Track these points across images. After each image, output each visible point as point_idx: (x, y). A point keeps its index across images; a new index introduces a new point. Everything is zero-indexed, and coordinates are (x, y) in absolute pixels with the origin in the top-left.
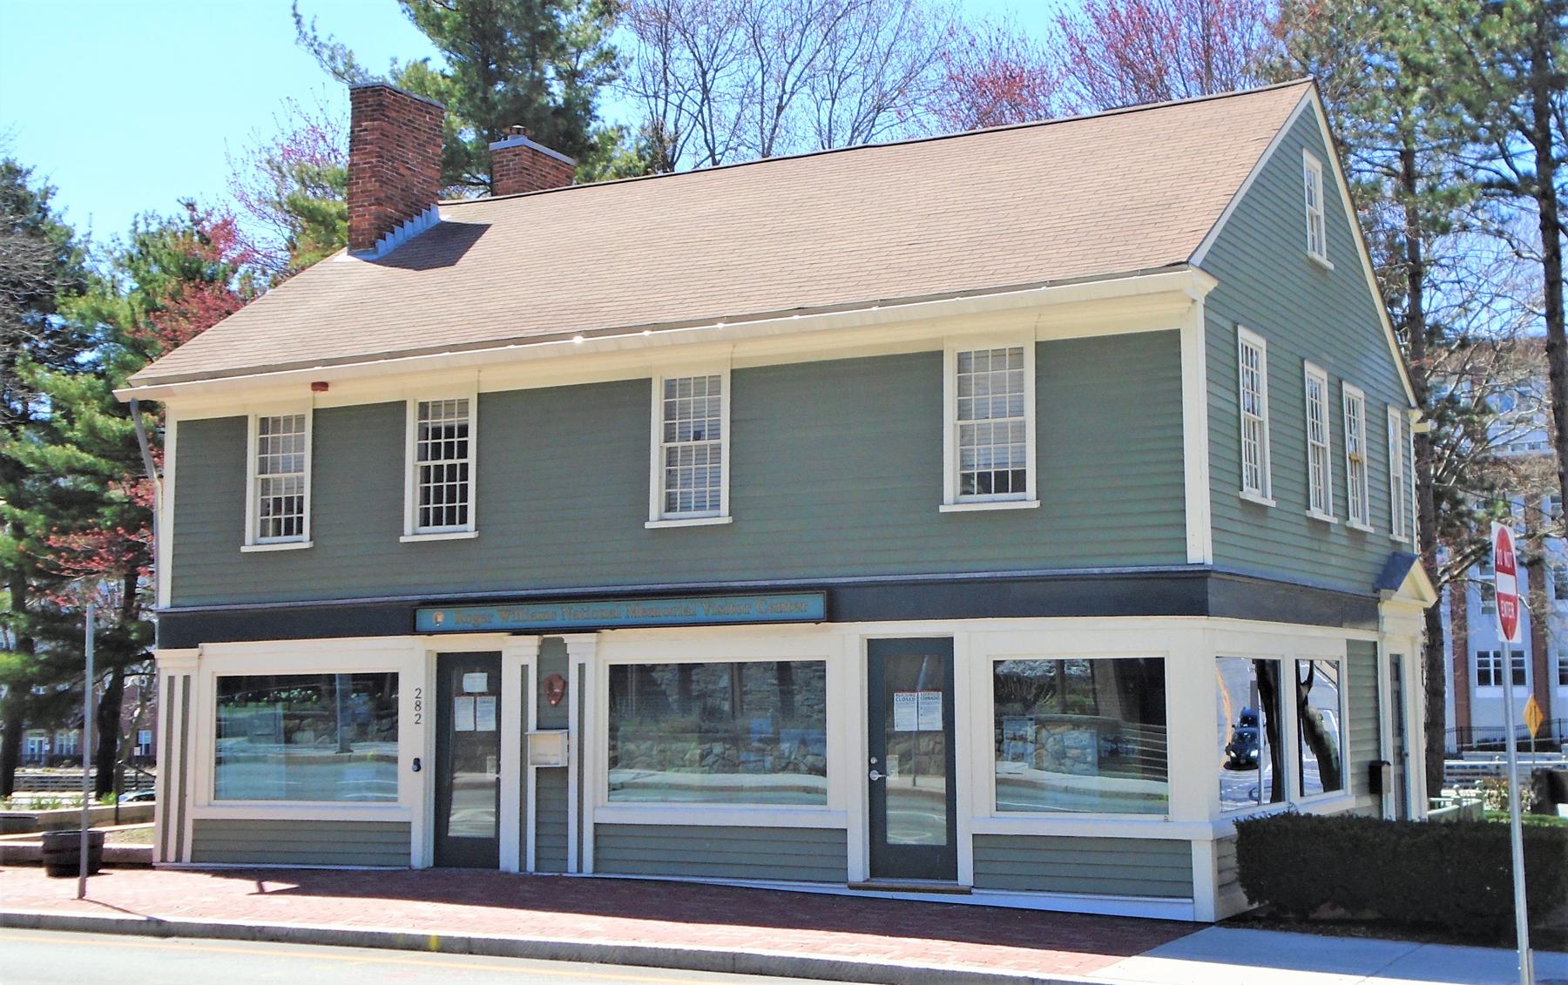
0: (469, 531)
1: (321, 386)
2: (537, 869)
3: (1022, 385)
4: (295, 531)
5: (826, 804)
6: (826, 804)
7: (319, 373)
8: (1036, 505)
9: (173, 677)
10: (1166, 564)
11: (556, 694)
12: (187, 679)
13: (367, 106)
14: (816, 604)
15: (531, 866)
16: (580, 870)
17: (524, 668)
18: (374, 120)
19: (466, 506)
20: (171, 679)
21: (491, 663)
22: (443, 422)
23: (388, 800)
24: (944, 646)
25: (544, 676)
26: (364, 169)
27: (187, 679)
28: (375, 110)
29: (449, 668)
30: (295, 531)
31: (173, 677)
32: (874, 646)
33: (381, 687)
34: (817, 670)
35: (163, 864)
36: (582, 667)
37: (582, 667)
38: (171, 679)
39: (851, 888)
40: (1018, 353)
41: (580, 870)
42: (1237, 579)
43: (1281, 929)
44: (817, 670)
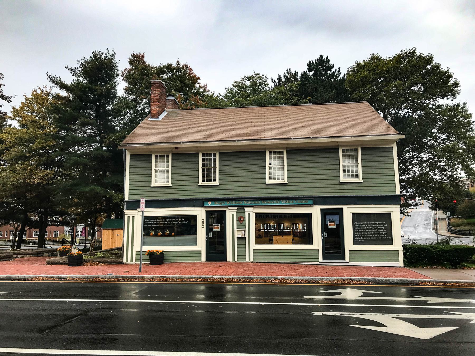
0: (201, 183)
2: (237, 261)
10: (392, 194)
11: (242, 221)
14: (310, 202)
15: (236, 260)
16: (250, 260)
17: (233, 215)
18: (158, 89)
20: (129, 217)
24: (342, 209)
26: (155, 100)
27: (133, 217)
29: (324, 213)
32: (322, 210)
36: (249, 214)
37: (249, 214)
38: (129, 217)
41: (250, 260)
42: (376, 267)
43: (435, 268)
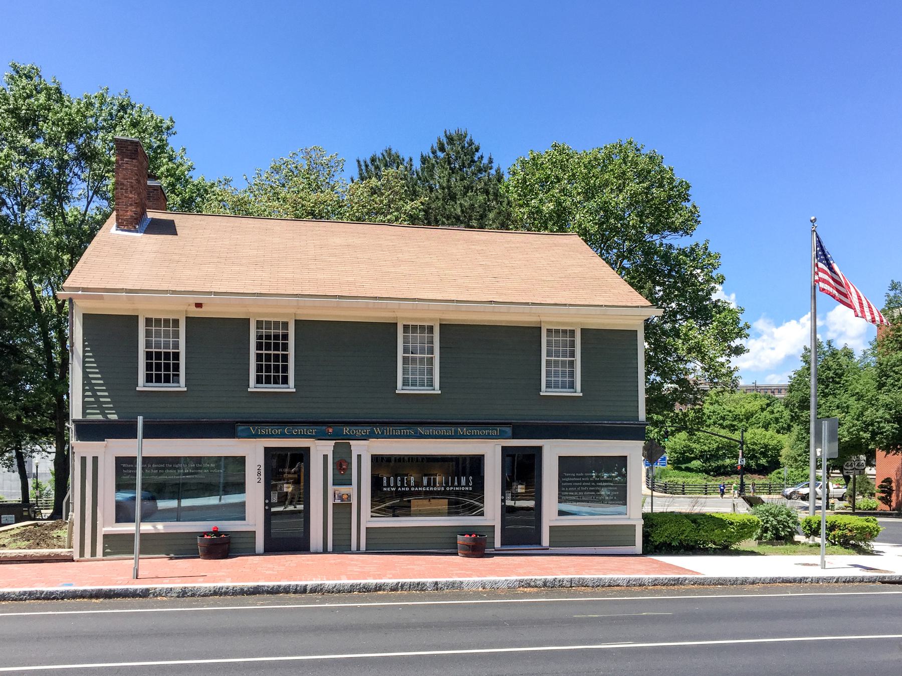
0: (291, 387)
1: (199, 305)
3: (433, 342)
4: (171, 381)
5: (245, 520)
6: (245, 520)
7: (199, 299)
8: (185, 389)
9: (97, 457)
12: (95, 459)
13: (126, 150)
17: (325, 457)
19: (287, 376)
21: (302, 456)
22: (272, 332)
23: (620, 514)
25: (337, 460)
27: (95, 459)
28: (133, 153)
30: (171, 381)
31: (97, 457)
33: (475, 465)
34: (562, 459)
35: (82, 558)
36: (359, 456)
37: (359, 456)
38: (83, 459)
39: (495, 550)
40: (176, 322)
44: (562, 459)
